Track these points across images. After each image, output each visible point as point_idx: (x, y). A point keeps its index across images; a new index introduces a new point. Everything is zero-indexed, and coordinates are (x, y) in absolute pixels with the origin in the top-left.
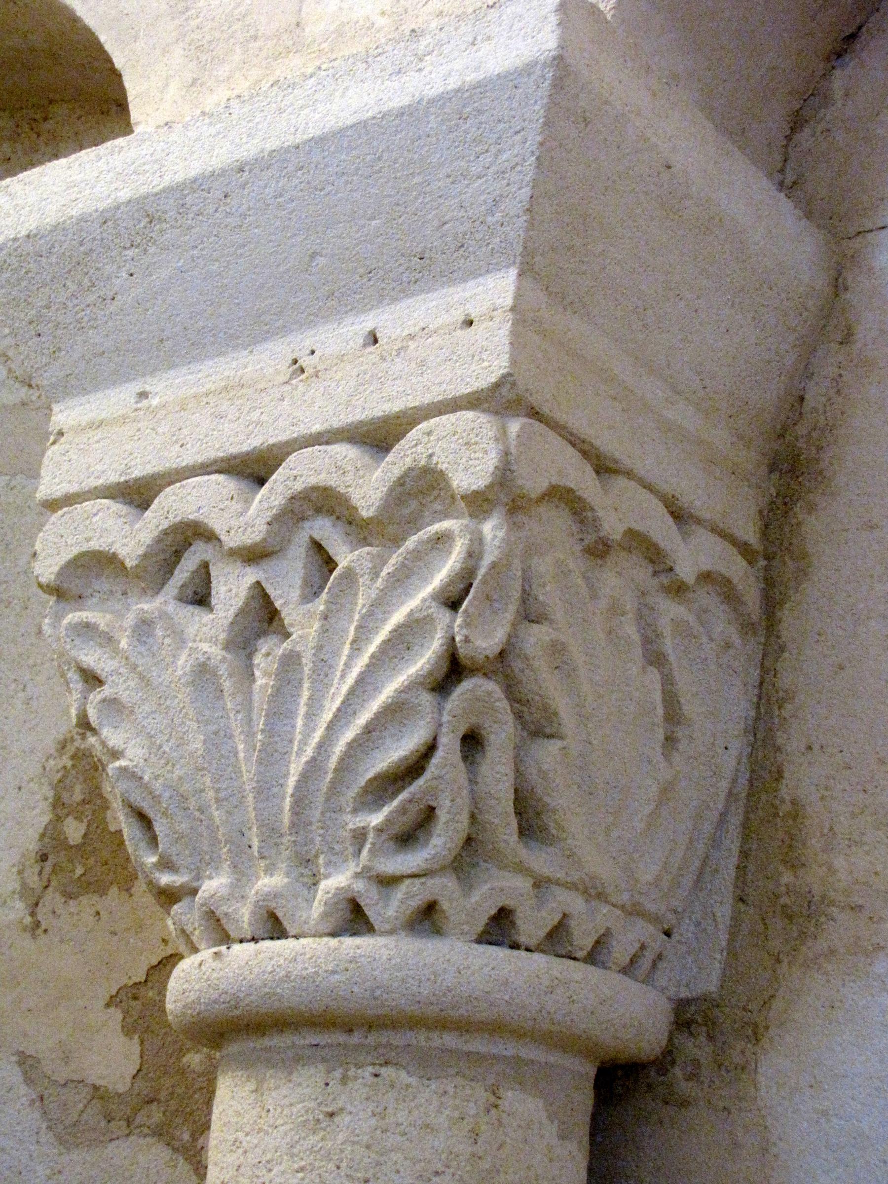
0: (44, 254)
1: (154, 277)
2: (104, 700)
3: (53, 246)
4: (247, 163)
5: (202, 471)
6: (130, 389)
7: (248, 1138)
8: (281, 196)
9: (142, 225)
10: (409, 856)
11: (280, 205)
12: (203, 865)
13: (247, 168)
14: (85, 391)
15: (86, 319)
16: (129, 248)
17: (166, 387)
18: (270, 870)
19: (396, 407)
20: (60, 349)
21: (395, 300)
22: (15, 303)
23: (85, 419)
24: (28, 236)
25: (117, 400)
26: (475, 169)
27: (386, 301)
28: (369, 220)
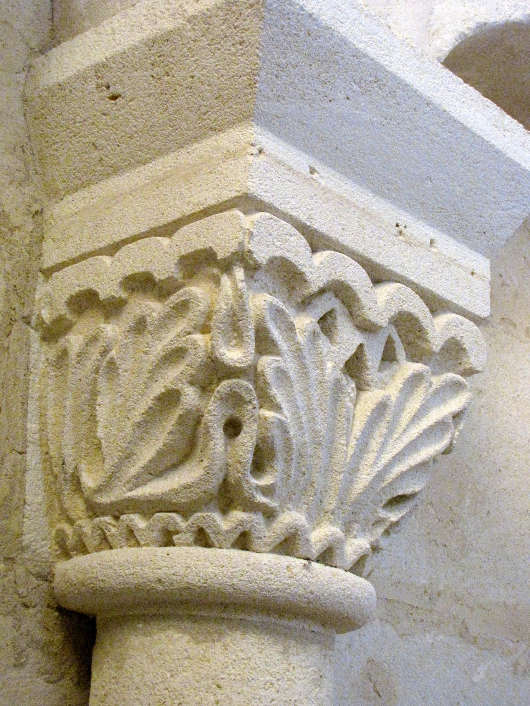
0: (312, 35)
1: (357, 112)
2: (278, 368)
3: (319, 37)
4: (432, 104)
5: (301, 229)
6: (311, 161)
7: (280, 683)
8: (436, 136)
9: (371, 79)
10: (188, 465)
11: (432, 140)
12: (291, 499)
13: (431, 106)
14: (278, 134)
15: (309, 96)
16: (356, 83)
17: (327, 177)
18: (333, 523)
19: (448, 296)
20: (284, 98)
21: (443, 231)
22: (277, 44)
23: (281, 156)
24: (310, 15)
25: (301, 161)
26: (503, 205)
27: (439, 228)
28: (459, 186)
